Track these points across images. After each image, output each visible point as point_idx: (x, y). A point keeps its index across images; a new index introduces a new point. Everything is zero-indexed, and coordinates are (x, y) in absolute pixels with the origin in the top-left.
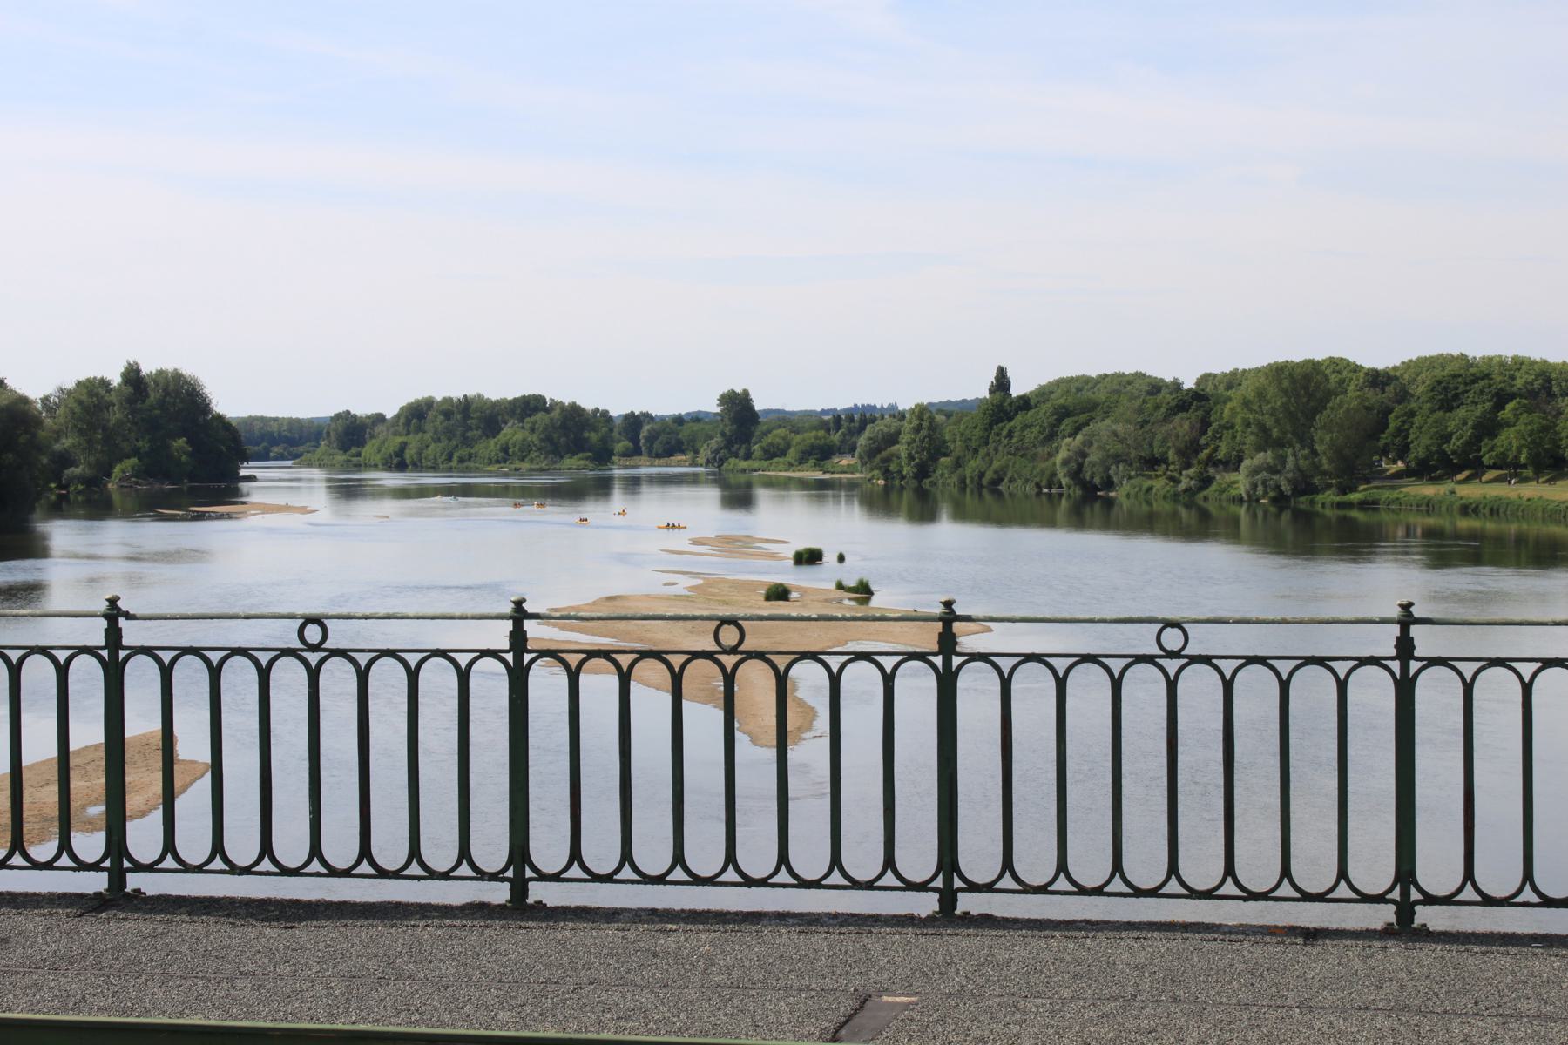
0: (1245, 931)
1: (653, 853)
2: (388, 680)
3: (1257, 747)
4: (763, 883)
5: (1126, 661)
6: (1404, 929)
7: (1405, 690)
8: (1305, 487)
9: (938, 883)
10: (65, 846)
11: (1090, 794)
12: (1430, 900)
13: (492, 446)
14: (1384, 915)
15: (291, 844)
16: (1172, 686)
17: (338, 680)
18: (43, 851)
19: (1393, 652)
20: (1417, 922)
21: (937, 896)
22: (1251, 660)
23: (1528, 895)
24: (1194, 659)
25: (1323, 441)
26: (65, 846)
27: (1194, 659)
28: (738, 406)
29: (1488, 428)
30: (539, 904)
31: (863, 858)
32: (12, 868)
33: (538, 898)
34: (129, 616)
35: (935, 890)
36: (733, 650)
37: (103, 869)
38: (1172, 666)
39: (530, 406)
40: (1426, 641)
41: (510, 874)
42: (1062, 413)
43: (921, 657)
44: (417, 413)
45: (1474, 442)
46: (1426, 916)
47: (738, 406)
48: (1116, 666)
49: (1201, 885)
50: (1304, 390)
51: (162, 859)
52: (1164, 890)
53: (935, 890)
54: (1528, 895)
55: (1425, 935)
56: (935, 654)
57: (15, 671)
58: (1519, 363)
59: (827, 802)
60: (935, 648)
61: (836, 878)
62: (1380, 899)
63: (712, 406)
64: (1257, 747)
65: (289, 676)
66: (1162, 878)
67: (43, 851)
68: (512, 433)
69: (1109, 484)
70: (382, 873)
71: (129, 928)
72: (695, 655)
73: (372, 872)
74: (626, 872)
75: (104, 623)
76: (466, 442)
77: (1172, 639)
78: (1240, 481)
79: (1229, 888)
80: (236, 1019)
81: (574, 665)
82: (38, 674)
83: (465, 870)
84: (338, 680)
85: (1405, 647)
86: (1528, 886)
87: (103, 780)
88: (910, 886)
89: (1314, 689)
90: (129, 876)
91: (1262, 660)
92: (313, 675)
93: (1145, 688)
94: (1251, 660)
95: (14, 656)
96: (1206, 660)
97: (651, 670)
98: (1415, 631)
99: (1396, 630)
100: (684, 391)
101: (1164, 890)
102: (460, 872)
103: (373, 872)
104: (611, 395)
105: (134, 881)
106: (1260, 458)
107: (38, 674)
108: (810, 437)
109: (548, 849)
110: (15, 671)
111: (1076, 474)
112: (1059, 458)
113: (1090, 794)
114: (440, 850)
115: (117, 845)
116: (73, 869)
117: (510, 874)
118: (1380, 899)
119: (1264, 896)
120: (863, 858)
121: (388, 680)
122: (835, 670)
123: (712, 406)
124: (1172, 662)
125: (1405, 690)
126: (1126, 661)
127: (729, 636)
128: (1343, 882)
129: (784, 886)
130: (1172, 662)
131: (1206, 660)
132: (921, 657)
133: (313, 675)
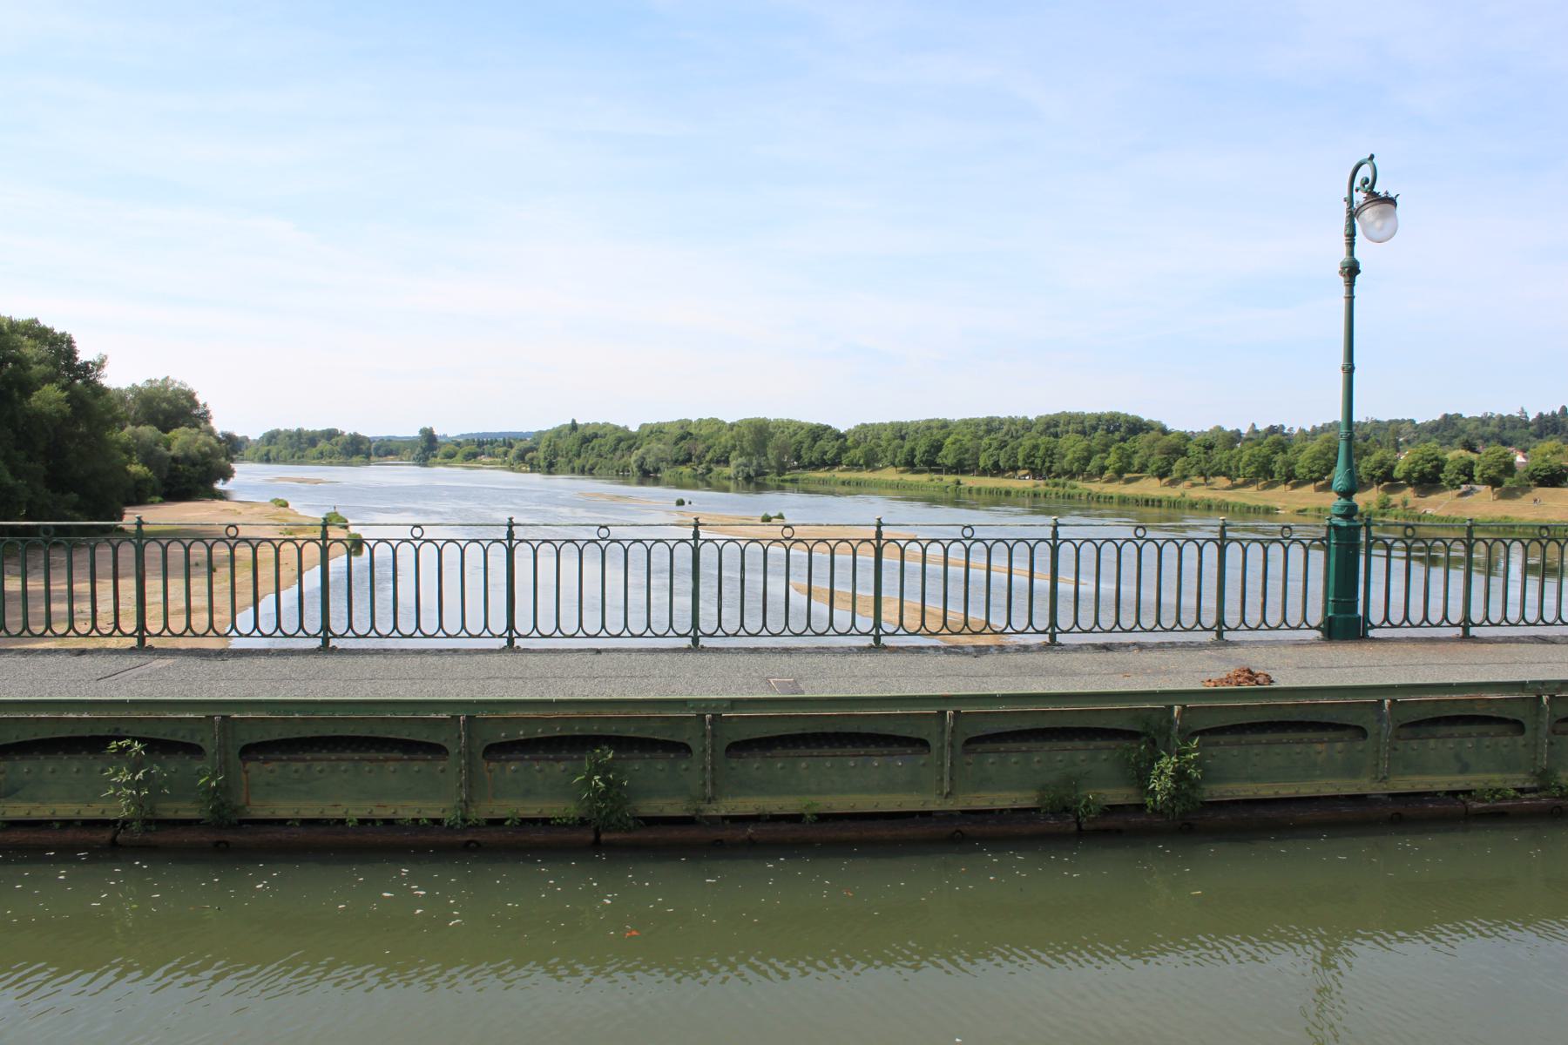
0: (468, 652)
6: (696, 647)
8: (760, 473)
10: (71, 627)
13: (314, 451)
14: (318, 643)
16: (417, 551)
18: (60, 628)
22: (635, 541)
23: (720, 633)
25: (772, 454)
26: (71, 627)
29: (843, 450)
30: (334, 648)
31: (475, 625)
38: (1140, 542)
39: (331, 434)
40: (519, 533)
42: (620, 440)
43: (499, 541)
44: (272, 437)
45: (838, 455)
46: (703, 642)
48: (1032, 543)
50: (760, 433)
54: (671, 633)
55: (703, 650)
58: (790, 422)
61: (441, 634)
62: (686, 635)
63: (417, 434)
67: (60, 628)
68: (323, 445)
69: (657, 470)
71: (1467, 647)
72: (1128, 540)
76: (303, 450)
77: (417, 532)
78: (730, 471)
79: (558, 634)
83: (278, 633)
85: (879, 535)
91: (477, 541)
93: (956, 552)
94: (635, 541)
97: (1109, 546)
98: (700, 529)
100: (409, 429)
104: (371, 429)
105: (149, 641)
106: (740, 460)
108: (467, 449)
111: (640, 467)
112: (634, 458)
115: (325, 627)
118: (686, 635)
119: (432, 636)
120: (475, 625)
123: (417, 434)
127: (417, 532)
133: (1286, 550)
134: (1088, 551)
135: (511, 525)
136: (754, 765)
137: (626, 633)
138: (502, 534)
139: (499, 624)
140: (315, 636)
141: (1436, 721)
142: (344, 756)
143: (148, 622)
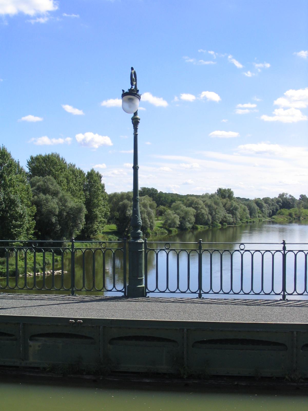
3: (247, 268)
7: (284, 256)
11: (237, 275)
19: (282, 249)
21: (198, 294)
24: (246, 251)
27: (246, 251)
38: (242, 252)
51: (294, 292)
59: (230, 271)
62: (195, 293)
64: (247, 268)
74: (252, 293)
85: (284, 248)
86: (306, 291)
87: (9, 262)
89: (268, 256)
96: (249, 251)
98: (286, 245)
99: (283, 245)
113: (237, 275)
118: (195, 293)
125: (284, 256)
131: (249, 251)
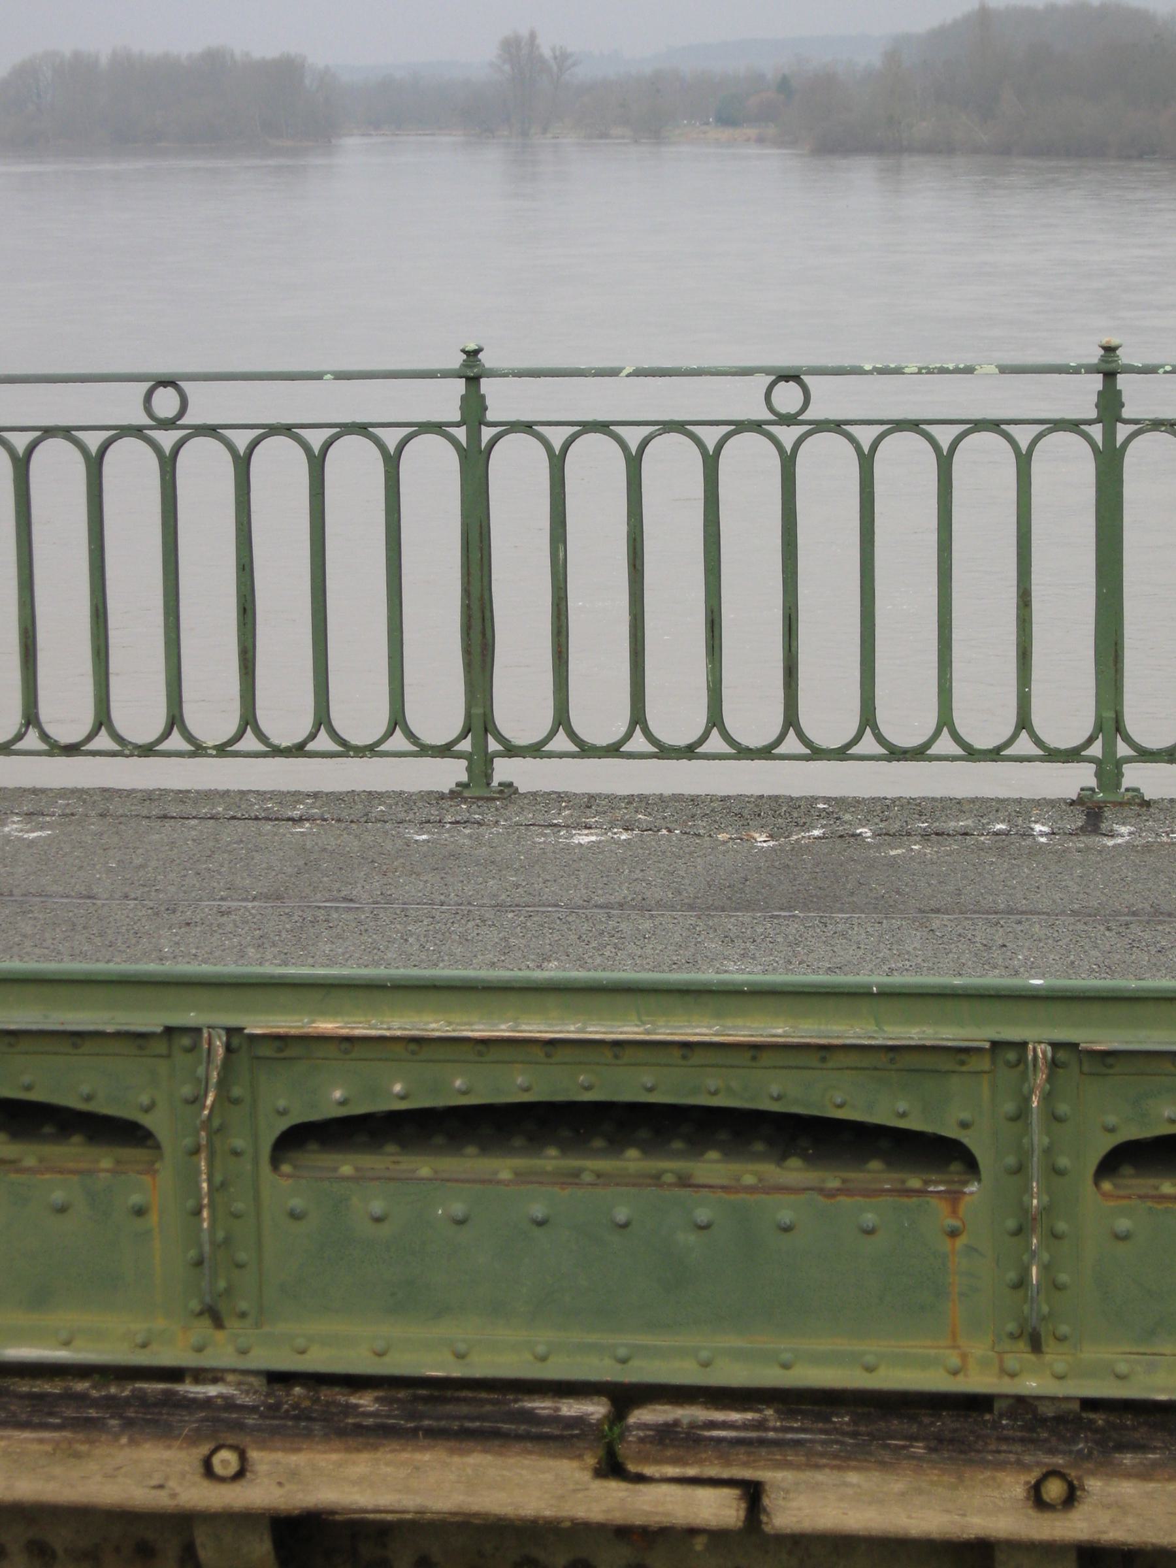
1: (677, 714)
2: (280, 470)
4: (995, 755)
5: (959, 429)
6: (480, 789)
9: (1096, 750)
12: (511, 751)
14: (449, 774)
15: (286, 712)
17: (205, 471)
20: (1126, 783)
21: (464, 763)
24: (821, 426)
27: (821, 426)
28: (520, 54)
30: (508, 787)
31: (360, 711)
32: (550, 755)
33: (506, 779)
34: (492, 374)
35: (1090, 760)
36: (788, 420)
37: (459, 756)
40: (1140, 398)
41: (1096, 750)
43: (436, 428)
47: (520, 54)
49: (907, 740)
52: (310, 747)
53: (1090, 760)
56: (457, 425)
57: (22, 465)
60: (1093, 414)
61: (561, 742)
65: (131, 471)
66: (623, 729)
70: (348, 750)
72: (741, 427)
73: (727, 749)
75: (460, 385)
80: (918, 969)
81: (93, 449)
82: (58, 473)
84: (205, 471)
85: (474, 409)
88: (1053, 755)
90: (1127, 769)
91: (914, 425)
92: (168, 464)
95: (20, 441)
96: (837, 426)
99: (1096, 382)
101: (781, 750)
102: (554, 745)
103: (574, 748)
105: (504, 770)
107: (58, 473)
109: (520, 707)
110: (22, 465)
114: (360, 711)
115: (480, 719)
116: (1041, 759)
117: (466, 745)
121: (280, 470)
122: (945, 447)
124: (787, 429)
126: (959, 429)
127: (788, 397)
128: (1024, 734)
129: (562, 755)
130: (787, 429)
132: (1074, 426)
133: (168, 464)
134: (596, 468)
135: (1109, 368)
136: (375, 1190)
137: (32, 740)
138: (1080, 397)
139: (439, 709)
140: (445, 751)
141: (828, 994)
142: (857, 1177)
143: (186, 708)
